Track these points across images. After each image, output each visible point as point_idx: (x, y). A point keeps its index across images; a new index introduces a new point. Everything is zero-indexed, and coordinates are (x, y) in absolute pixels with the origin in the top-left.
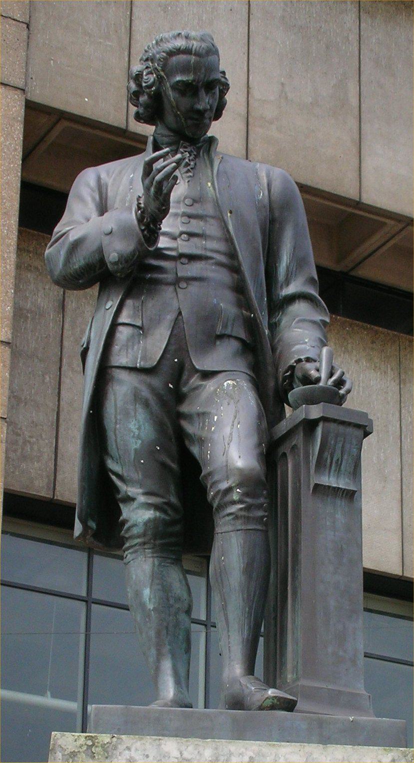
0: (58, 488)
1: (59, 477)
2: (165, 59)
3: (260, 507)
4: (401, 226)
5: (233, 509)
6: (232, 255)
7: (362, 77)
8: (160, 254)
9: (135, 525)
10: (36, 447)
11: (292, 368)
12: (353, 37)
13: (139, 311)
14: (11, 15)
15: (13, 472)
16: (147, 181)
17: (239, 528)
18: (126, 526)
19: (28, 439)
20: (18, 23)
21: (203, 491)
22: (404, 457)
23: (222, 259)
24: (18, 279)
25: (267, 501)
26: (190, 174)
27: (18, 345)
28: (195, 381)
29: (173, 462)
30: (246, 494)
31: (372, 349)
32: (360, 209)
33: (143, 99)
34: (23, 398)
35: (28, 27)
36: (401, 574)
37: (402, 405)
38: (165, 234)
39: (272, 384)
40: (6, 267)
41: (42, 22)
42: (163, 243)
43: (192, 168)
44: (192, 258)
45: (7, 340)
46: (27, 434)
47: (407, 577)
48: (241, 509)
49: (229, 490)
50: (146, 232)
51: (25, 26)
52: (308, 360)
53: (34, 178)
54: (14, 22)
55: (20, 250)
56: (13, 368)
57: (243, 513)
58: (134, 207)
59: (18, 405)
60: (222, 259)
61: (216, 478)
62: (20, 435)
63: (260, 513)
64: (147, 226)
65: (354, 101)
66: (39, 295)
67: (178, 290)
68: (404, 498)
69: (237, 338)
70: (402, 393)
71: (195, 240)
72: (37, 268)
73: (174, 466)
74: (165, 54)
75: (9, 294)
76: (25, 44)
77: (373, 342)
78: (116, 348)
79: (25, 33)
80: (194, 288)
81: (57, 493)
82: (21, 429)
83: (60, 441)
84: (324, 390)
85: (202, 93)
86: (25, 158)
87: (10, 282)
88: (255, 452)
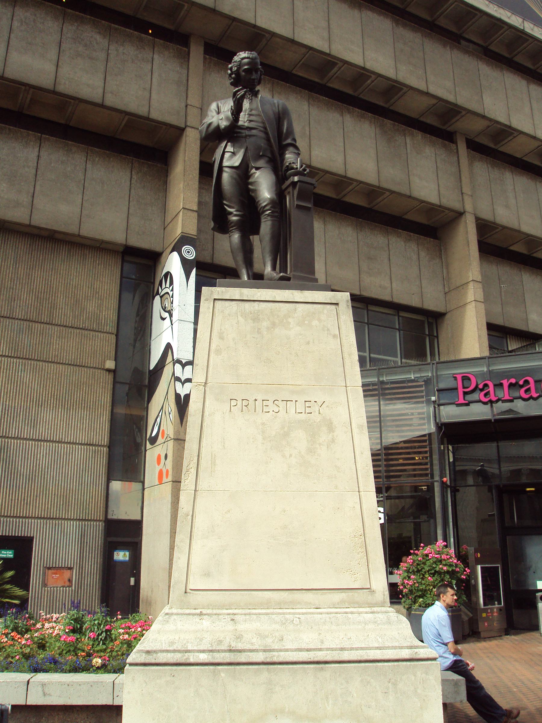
3: (277, 212)
6: (265, 128)
8: (241, 128)
9: (232, 223)
11: (287, 166)
12: (307, 113)
13: (233, 146)
23: (262, 129)
24: (200, 193)
28: (254, 170)
30: (271, 207)
33: (233, 76)
39: (280, 173)
42: (240, 123)
52: (293, 163)
60: (262, 129)
61: (261, 202)
63: (276, 214)
64: (235, 117)
65: (308, 133)
69: (268, 157)
71: (252, 123)
78: (224, 160)
80: (252, 139)
84: (300, 171)
85: (254, 73)
86: (200, 154)
87: (197, 191)
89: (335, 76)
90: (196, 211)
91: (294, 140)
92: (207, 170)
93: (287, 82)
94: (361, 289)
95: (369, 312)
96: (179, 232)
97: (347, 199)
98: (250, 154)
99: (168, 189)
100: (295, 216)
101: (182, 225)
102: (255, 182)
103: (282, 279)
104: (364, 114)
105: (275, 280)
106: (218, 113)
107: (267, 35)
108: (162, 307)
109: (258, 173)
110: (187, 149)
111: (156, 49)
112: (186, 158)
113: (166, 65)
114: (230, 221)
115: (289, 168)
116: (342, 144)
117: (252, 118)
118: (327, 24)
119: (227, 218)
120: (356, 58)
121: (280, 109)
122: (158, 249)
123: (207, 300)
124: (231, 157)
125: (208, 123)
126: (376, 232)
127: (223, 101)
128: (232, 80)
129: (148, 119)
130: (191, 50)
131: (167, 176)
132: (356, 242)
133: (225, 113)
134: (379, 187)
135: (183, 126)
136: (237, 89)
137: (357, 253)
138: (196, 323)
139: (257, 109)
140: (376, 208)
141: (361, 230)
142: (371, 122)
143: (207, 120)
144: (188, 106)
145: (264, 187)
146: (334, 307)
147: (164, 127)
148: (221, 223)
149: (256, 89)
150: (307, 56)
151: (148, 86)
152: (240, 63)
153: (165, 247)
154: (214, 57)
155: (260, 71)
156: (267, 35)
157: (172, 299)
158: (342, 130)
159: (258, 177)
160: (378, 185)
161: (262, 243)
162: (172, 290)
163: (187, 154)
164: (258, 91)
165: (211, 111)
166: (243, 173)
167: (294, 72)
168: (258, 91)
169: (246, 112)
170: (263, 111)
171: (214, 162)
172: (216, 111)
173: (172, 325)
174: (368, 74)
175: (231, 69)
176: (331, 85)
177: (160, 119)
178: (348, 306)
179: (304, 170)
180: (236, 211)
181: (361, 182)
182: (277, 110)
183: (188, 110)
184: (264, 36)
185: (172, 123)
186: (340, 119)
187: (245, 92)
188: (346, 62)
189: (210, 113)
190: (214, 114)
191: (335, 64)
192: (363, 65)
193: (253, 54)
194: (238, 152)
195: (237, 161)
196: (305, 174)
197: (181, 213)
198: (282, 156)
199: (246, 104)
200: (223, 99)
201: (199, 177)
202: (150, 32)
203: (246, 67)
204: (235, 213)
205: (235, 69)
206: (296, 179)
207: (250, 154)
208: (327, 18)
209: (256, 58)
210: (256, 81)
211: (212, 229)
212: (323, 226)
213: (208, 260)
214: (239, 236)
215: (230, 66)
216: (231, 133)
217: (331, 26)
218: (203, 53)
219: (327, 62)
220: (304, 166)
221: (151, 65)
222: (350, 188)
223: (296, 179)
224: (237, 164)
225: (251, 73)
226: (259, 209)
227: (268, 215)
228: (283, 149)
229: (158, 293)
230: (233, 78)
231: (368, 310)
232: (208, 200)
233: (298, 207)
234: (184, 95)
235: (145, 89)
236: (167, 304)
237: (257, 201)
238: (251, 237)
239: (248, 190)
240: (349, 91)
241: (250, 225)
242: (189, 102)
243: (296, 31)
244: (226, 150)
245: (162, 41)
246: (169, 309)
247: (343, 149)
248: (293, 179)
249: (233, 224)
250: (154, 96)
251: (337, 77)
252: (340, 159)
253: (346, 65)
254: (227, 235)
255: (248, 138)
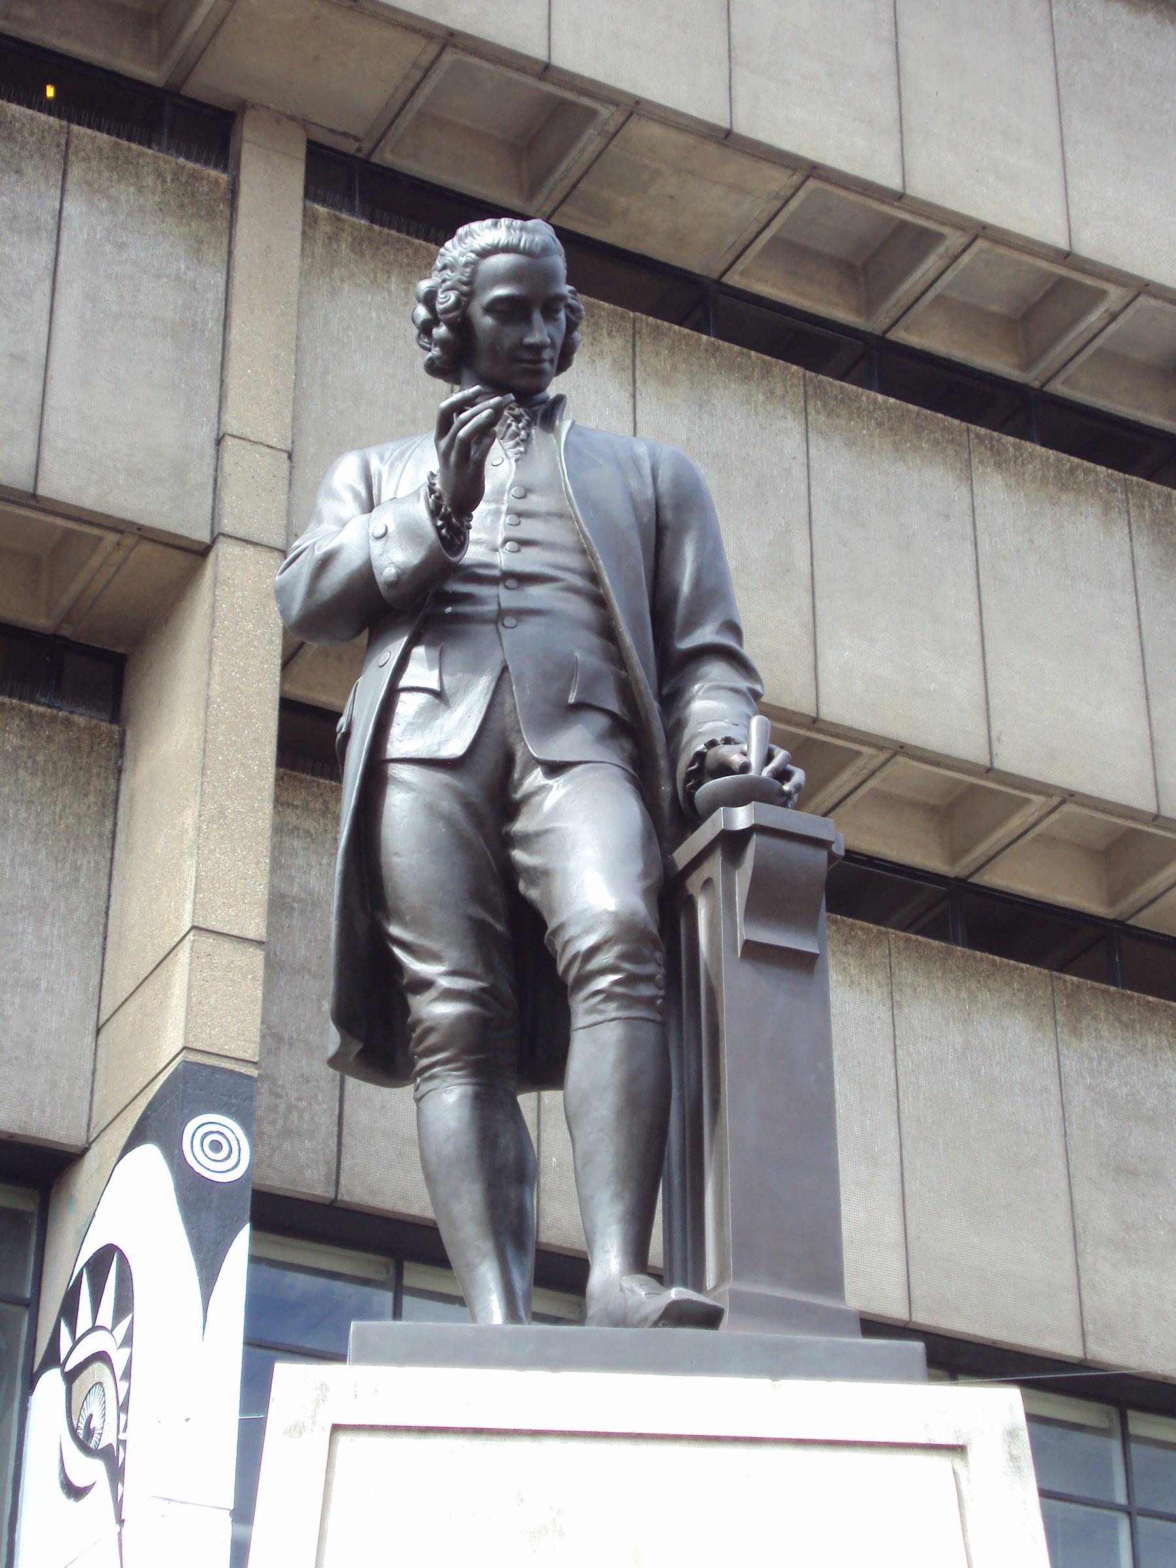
0: (343, 1181)
1: (346, 1163)
2: (473, 265)
3: (648, 979)
4: (883, 756)
5: (604, 982)
6: (594, 577)
7: (814, 529)
8: (472, 575)
9: (429, 1030)
10: (307, 1116)
11: (700, 756)
12: (798, 470)
14: (263, 439)
15: (270, 1157)
16: (444, 443)
17: (614, 1015)
18: (419, 1031)
19: (294, 1102)
20: (274, 452)
21: (552, 961)
22: (903, 1127)
23: (579, 581)
25: (663, 970)
26: (522, 449)
27: (278, 953)
28: (536, 778)
29: (498, 920)
30: (623, 956)
31: (846, 954)
32: (819, 731)
33: (441, 331)
34: (286, 1036)
35: (290, 457)
36: (906, 1317)
37: (898, 1042)
38: (477, 542)
39: (665, 788)
40: (256, 822)
41: (312, 450)
42: (473, 554)
43: (522, 440)
44: (525, 579)
45: (258, 938)
46: (293, 1095)
47: (919, 1324)
48: (616, 983)
49: (593, 951)
50: (444, 531)
51: (285, 456)
52: (728, 741)
53: (300, 693)
54: (268, 450)
55: (280, 802)
56: (269, 986)
57: (619, 990)
58: (424, 490)
59: (278, 1048)
60: (579, 581)
61: (570, 932)
62: (280, 1097)
63: (646, 991)
64: (446, 518)
65: (803, 565)
66: (313, 873)
67: (502, 629)
68: (907, 1192)
70: (896, 1023)
71: (526, 551)
72: (307, 832)
73: (500, 927)
74: (473, 256)
75: (262, 865)
76: (286, 482)
77: (846, 943)
78: (395, 731)
79: (286, 465)
80: (530, 629)
81: (342, 1189)
82: (283, 1086)
83: (347, 1106)
85: (537, 317)
87: (263, 845)
88: (639, 886)
89: (930, 295)
90: (260, 943)
91: (733, 628)
92: (307, 741)
93: (699, 328)
94: (1090, 1328)
95: (1134, 1448)
96: (168, 1045)
97: (998, 878)
98: (519, 697)
99: (121, 838)
100: (742, 997)
101: (189, 1009)
102: (539, 834)
103: (677, 1315)
104: (1072, 470)
105: (641, 1323)
106: (370, 505)
107: (604, 112)
108: (73, 1431)
109: (558, 790)
110: (218, 643)
111: (75, 172)
112: (216, 688)
113: (122, 246)
114: (419, 1022)
115: (704, 768)
116: (972, 616)
117: (529, 529)
118: (891, 56)
119: (406, 1010)
120: (1034, 216)
121: (664, 485)
122: (55, 1126)
123: (297, 1430)
124: (426, 717)
125: (319, 553)
126: (1151, 1040)
127: (390, 449)
128: (436, 352)
129: (32, 500)
130: (243, 177)
131: (120, 771)
132: (1054, 1089)
133: (404, 508)
134: (1156, 819)
135: (204, 536)
136: (457, 396)
137: (1058, 1148)
138: (243, 1512)
139: (553, 486)
140: (1144, 920)
141: (1074, 1031)
142: (1107, 507)
143: (316, 540)
144: (229, 442)
145: (587, 855)
146: (941, 1463)
147: (111, 538)
148: (375, 1027)
149: (552, 391)
150: (794, 204)
151: (34, 347)
152: (474, 273)
153: (99, 1121)
154: (351, 211)
155: (570, 307)
156: (604, 112)
157: (123, 1386)
158: (970, 547)
159: (556, 811)
160: (1151, 808)
161: (577, 1127)
162: (128, 1341)
163: (217, 669)
164: (560, 400)
165: (333, 495)
166: (489, 790)
167: (734, 279)
168: (560, 400)
169: (499, 501)
170: (583, 496)
171: (347, 735)
172: (356, 495)
173: (121, 1522)
174: (1089, 281)
175: (429, 299)
176: (914, 340)
177: (90, 499)
178: (1013, 1458)
179: (783, 775)
180: (453, 973)
181: (1069, 796)
182: (650, 493)
183: (228, 459)
184: (593, 113)
185: (146, 521)
186: (960, 496)
187: (498, 411)
188: (980, 231)
189: (327, 507)
190: (350, 508)
191: (923, 241)
192: (1063, 244)
193: (533, 231)
194: (466, 688)
195: (454, 734)
196: (788, 795)
197: (184, 955)
198: (672, 699)
199: (501, 466)
200: (391, 438)
201: (279, 779)
202: (50, 92)
203: (500, 291)
204: (445, 983)
205: (447, 299)
206: (742, 817)
207: (519, 697)
208: (887, 31)
209: (546, 250)
210: (547, 354)
211: (334, 1062)
212: (883, 1012)
213: (312, 1183)
214: (462, 1097)
215: (424, 286)
216: (428, 602)
217: (908, 65)
218: (300, 191)
219: (895, 235)
220: (780, 755)
221: (47, 248)
222: (1016, 823)
223: (742, 817)
224: (456, 748)
225: (526, 319)
226: (561, 968)
227: (608, 995)
228: (675, 670)
229: (53, 1358)
230: (443, 343)
231: (1126, 1438)
232: (314, 883)
233: (754, 952)
234: (210, 387)
235: (17, 358)
236: (100, 1413)
237: (552, 925)
238: (526, 1101)
239: (509, 874)
240: (1003, 365)
241: (520, 1036)
242: (232, 423)
243: (740, 91)
244: (404, 682)
245: (103, 138)
246: (108, 1438)
247: (976, 639)
248: (728, 819)
249: (431, 1040)
250: (60, 393)
251: (939, 298)
252: (963, 687)
253: (980, 244)
254: (407, 1091)
255: (509, 621)
